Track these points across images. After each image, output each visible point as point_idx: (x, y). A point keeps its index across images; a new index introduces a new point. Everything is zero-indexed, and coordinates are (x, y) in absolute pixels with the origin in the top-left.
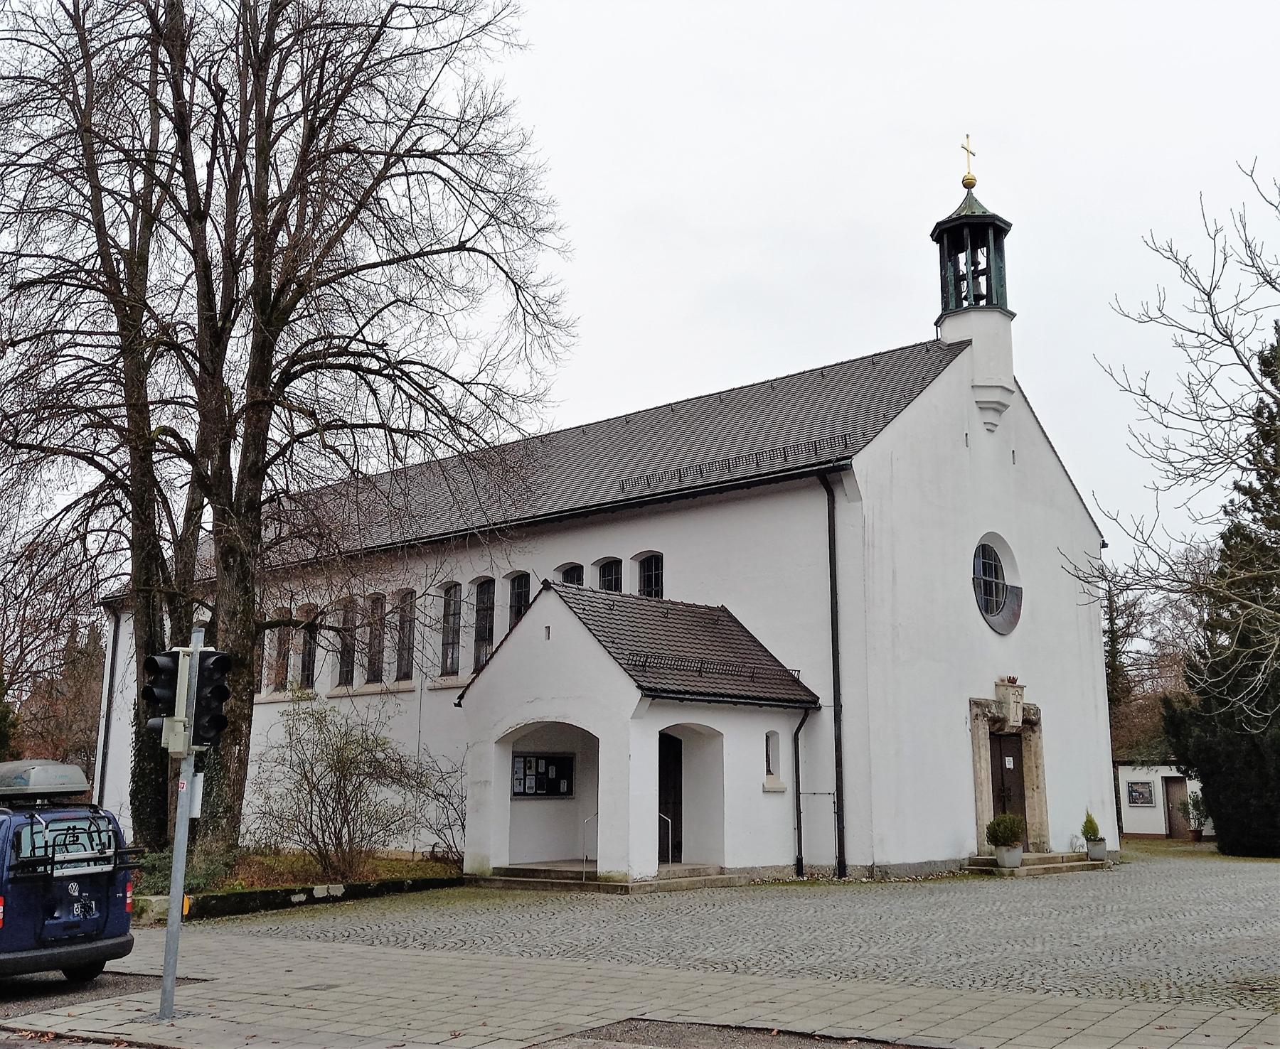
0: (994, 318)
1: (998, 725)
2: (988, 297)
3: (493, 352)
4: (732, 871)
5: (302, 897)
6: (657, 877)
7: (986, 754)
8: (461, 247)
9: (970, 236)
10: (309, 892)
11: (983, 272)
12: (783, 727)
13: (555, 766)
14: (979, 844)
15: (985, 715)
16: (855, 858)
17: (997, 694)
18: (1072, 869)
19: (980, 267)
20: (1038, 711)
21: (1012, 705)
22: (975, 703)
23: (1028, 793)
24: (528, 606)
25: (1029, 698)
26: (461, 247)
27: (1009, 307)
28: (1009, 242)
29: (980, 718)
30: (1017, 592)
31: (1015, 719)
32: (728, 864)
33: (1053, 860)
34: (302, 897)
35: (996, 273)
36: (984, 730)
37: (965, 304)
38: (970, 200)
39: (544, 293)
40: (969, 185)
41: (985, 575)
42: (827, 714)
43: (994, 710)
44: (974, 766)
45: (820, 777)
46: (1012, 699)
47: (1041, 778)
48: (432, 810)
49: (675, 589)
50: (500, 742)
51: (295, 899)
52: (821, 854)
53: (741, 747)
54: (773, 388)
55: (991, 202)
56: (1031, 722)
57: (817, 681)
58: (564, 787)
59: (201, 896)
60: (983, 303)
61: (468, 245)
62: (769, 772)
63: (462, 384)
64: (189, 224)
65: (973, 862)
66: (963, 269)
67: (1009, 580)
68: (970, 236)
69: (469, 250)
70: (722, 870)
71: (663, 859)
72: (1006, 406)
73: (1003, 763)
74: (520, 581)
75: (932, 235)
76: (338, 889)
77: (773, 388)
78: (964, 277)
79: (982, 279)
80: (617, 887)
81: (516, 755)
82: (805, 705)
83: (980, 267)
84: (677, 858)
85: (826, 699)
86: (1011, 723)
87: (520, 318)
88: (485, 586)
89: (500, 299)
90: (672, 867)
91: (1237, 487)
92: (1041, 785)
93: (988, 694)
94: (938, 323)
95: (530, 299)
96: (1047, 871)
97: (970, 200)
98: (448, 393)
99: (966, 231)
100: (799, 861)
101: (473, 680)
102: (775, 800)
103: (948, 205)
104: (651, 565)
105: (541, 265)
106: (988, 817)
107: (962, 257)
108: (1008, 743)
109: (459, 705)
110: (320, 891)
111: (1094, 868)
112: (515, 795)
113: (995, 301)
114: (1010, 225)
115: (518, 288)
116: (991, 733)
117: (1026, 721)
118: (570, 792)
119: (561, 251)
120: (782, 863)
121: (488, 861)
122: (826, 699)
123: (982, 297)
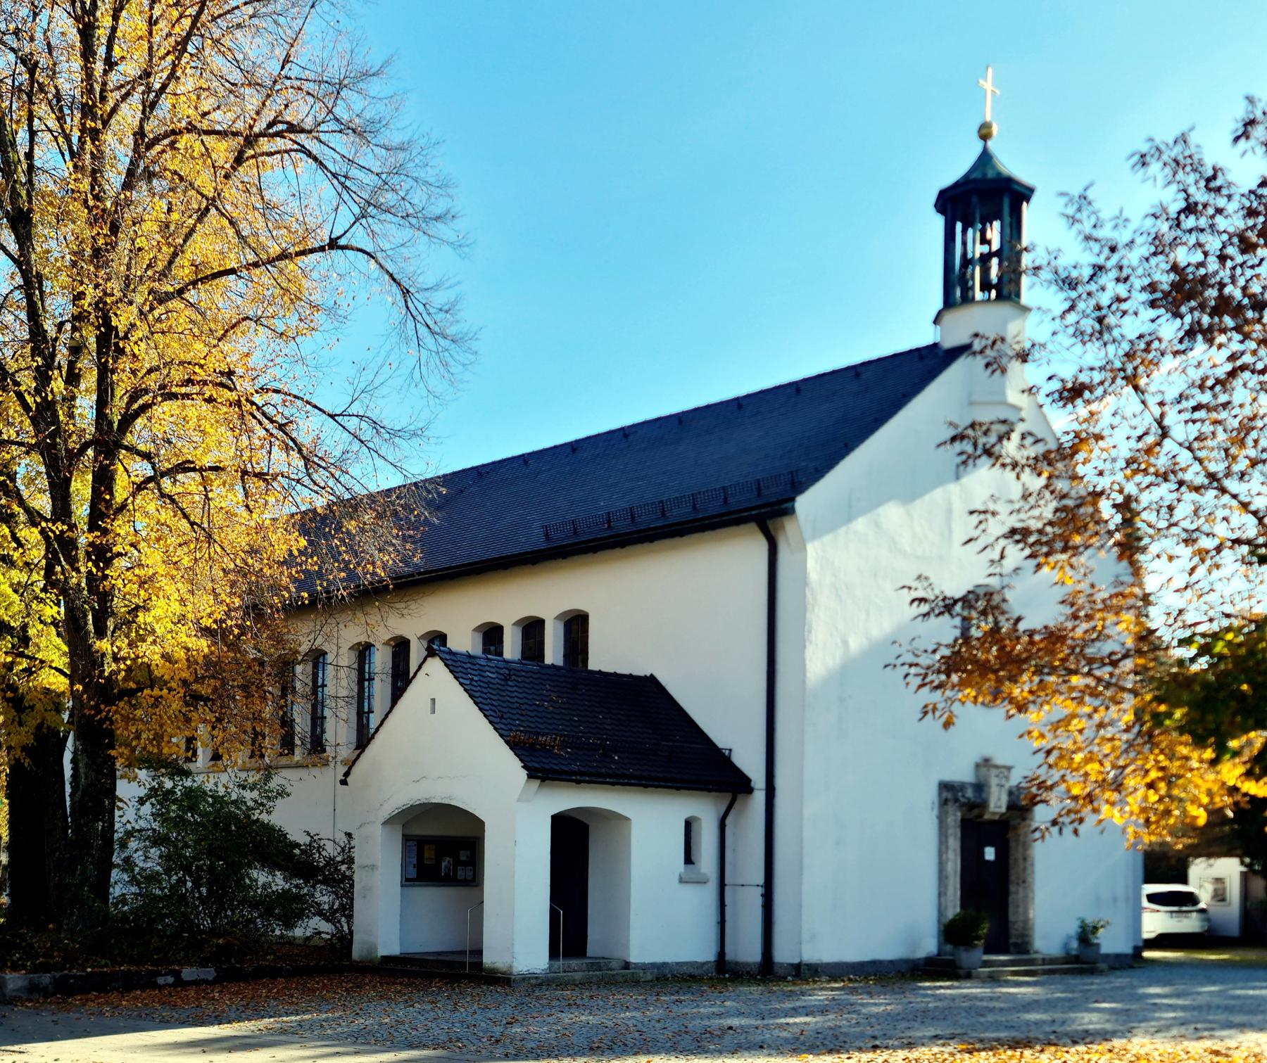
1: (976, 812)
2: (998, 287)
3: (368, 376)
5: (170, 980)
7: (954, 844)
8: (333, 244)
10: (177, 975)
12: (704, 809)
13: (445, 849)
15: (956, 800)
16: (784, 954)
17: (977, 776)
22: (945, 787)
23: (1012, 888)
26: (333, 244)
29: (950, 804)
32: (635, 957)
34: (170, 980)
36: (954, 817)
38: (985, 158)
39: (439, 299)
40: (985, 133)
43: (970, 793)
45: (749, 867)
46: (994, 782)
47: (1029, 871)
48: (324, 897)
49: (601, 658)
50: (389, 822)
51: (161, 981)
53: (651, 827)
57: (750, 762)
59: (58, 975)
61: (342, 242)
63: (332, 416)
64: (14, 229)
69: (343, 248)
70: (627, 965)
74: (400, 647)
76: (210, 973)
80: (500, 980)
81: (406, 839)
85: (758, 780)
87: (411, 332)
88: (363, 651)
89: (375, 309)
92: (1029, 880)
94: (937, 321)
95: (421, 308)
97: (985, 158)
98: (308, 428)
99: (975, 199)
100: (721, 953)
101: (358, 756)
102: (690, 892)
103: (955, 166)
104: (576, 625)
105: (427, 262)
109: (344, 782)
110: (188, 973)
112: (407, 882)
114: (1031, 190)
115: (406, 292)
116: (963, 821)
117: (1012, 806)
119: (457, 246)
120: (701, 958)
121: (376, 948)
122: (758, 780)
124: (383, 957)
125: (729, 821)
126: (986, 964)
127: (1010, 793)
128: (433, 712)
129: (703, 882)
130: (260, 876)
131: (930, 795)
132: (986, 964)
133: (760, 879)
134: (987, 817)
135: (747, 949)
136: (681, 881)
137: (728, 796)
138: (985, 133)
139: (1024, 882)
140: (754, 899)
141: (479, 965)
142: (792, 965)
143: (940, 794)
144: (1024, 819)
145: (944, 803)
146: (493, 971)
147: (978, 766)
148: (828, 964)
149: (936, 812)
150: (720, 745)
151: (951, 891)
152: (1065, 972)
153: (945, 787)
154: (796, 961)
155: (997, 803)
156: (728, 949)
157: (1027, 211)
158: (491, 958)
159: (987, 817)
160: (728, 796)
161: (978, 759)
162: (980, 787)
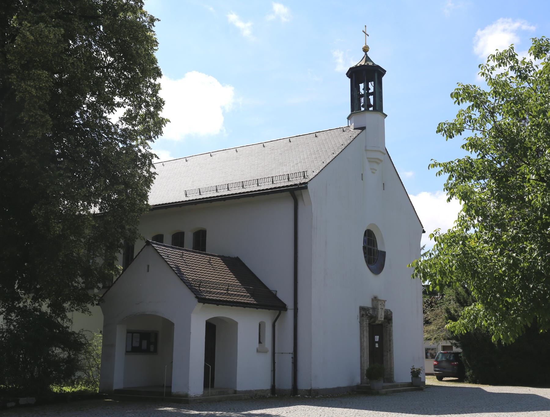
0: (377, 115)
1: (372, 320)
4: (240, 392)
5: (13, 404)
6: (203, 395)
7: (366, 334)
9: (366, 77)
11: (371, 94)
12: (266, 317)
14: (362, 379)
15: (367, 315)
16: (303, 385)
18: (406, 391)
19: (370, 91)
20: (391, 313)
21: (380, 310)
22: (362, 309)
24: (133, 260)
25: (388, 306)
27: (384, 111)
28: (385, 79)
30: (383, 254)
31: (381, 316)
32: (239, 388)
33: (397, 386)
34: (13, 404)
35: (378, 94)
36: (366, 323)
37: (363, 109)
38: (368, 59)
40: (366, 50)
41: (368, 244)
42: (290, 313)
43: (371, 312)
44: (361, 339)
46: (380, 307)
52: (286, 383)
54: (264, 146)
55: (377, 59)
56: (388, 318)
58: (152, 348)
60: (371, 109)
62: (260, 342)
65: (358, 387)
66: (362, 92)
67: (380, 248)
68: (366, 77)
70: (235, 392)
71: (206, 386)
72: (381, 161)
73: (374, 339)
75: (347, 74)
76: (32, 400)
77: (264, 146)
78: (362, 96)
79: (371, 98)
80: (183, 401)
81: (128, 332)
82: (280, 307)
83: (370, 91)
84: (212, 386)
85: (290, 304)
86: (379, 319)
90: (210, 390)
91: (473, 110)
93: (368, 304)
96: (394, 392)
100: (273, 386)
103: (356, 61)
106: (366, 365)
107: (362, 86)
108: (377, 326)
111: (415, 390)
112: (127, 352)
113: (378, 107)
116: (369, 324)
118: (155, 351)
122: (290, 304)
123: (371, 106)
124: (115, 390)
125: (276, 324)
126: (384, 388)
127: (385, 312)
128: (148, 271)
129: (266, 352)
130: (57, 351)
131: (357, 313)
132: (384, 388)
133: (291, 350)
134: (377, 322)
135: (286, 383)
136: (258, 351)
137: (278, 312)
138: (366, 50)
139: (390, 351)
140: (289, 359)
141: (169, 393)
142: (307, 390)
143: (360, 312)
144: (389, 323)
145: (362, 316)
146: (179, 396)
147: (373, 300)
148: (321, 389)
149: (359, 320)
150: (271, 289)
151: (365, 353)
152: (412, 390)
153: (362, 309)
154: (309, 388)
155: (381, 316)
156: (342, 382)
157: (384, 79)
158: (175, 390)
159: (377, 322)
160: (278, 312)
161: (373, 297)
162: (375, 309)
